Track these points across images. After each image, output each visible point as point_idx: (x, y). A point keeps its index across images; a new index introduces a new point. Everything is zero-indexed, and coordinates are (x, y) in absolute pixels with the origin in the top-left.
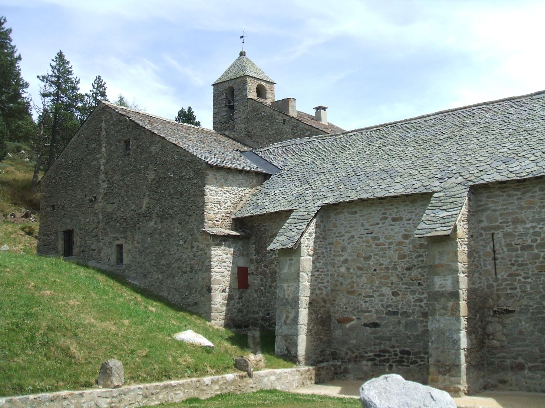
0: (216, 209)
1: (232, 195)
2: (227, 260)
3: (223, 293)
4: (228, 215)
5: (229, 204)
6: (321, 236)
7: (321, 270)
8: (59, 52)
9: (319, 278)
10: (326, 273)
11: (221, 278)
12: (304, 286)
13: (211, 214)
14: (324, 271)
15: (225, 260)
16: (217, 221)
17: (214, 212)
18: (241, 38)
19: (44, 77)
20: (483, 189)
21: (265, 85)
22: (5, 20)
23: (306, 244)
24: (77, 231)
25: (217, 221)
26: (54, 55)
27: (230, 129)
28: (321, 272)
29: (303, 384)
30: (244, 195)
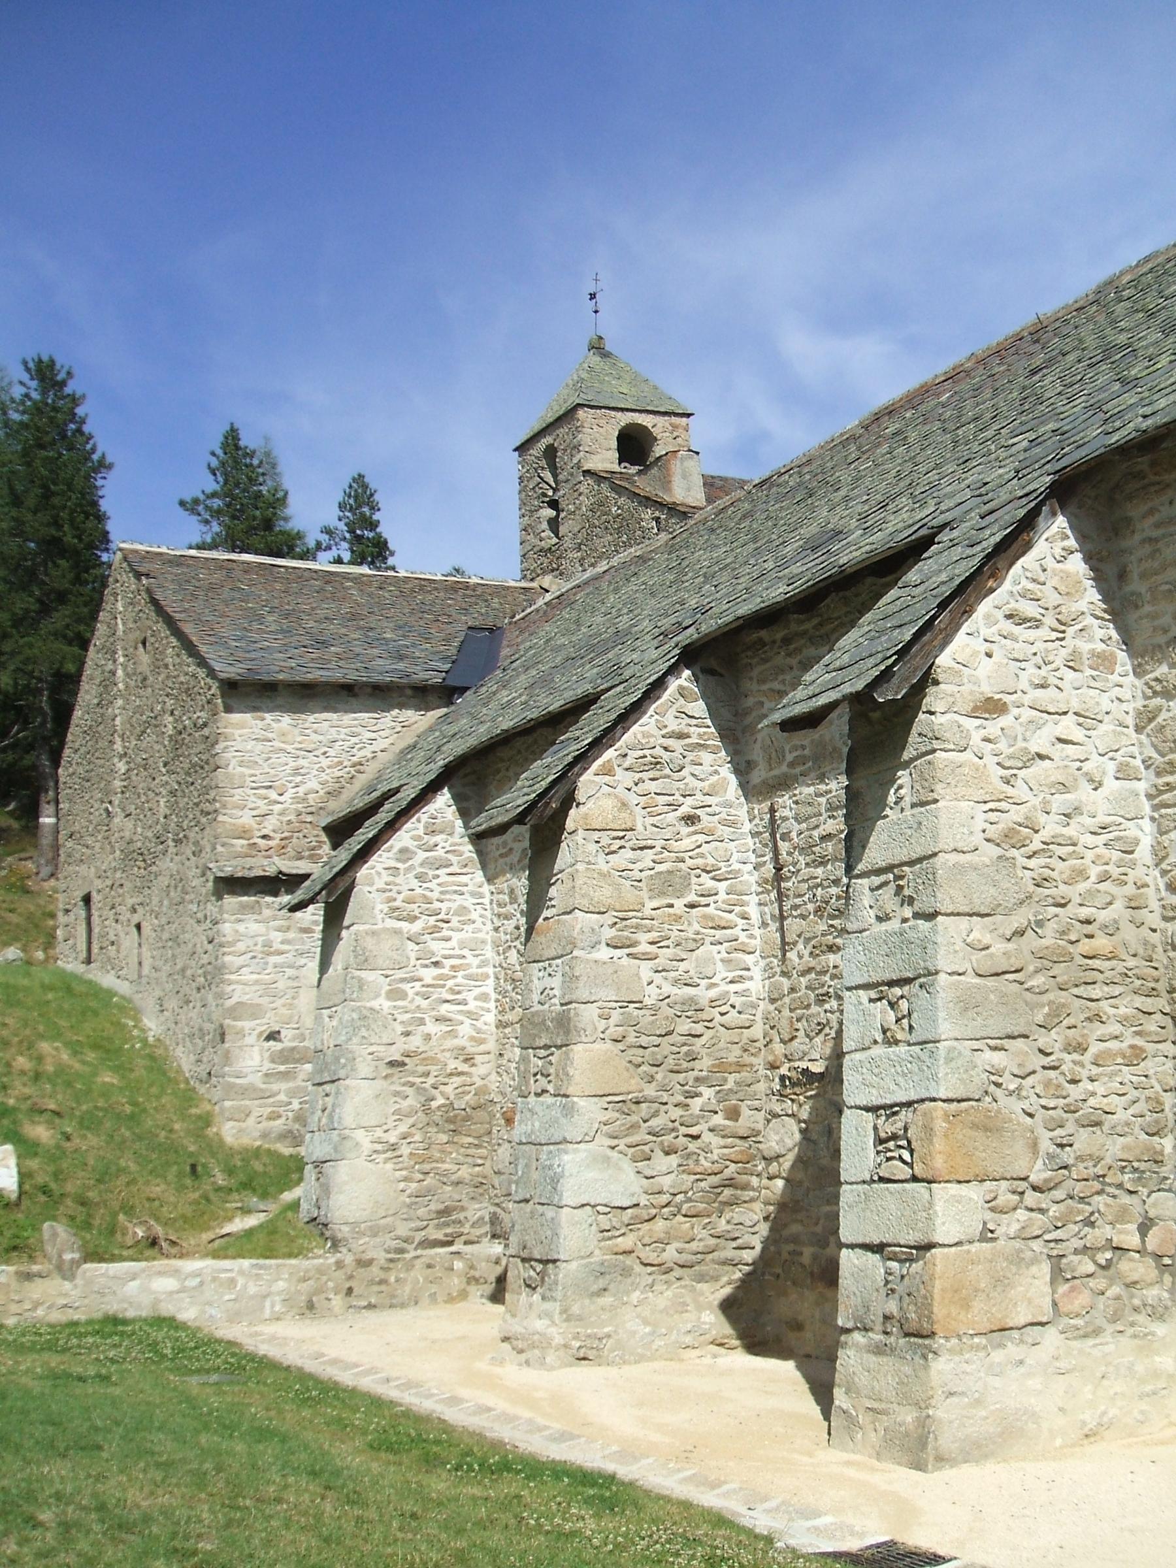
0: (261, 803)
1: (322, 758)
2: (285, 947)
3: (272, 1043)
4: (309, 818)
5: (313, 784)
6: (454, 859)
7: (448, 963)
8: (228, 428)
9: (443, 986)
10: (474, 970)
11: (264, 1001)
12: (365, 1012)
13: (246, 819)
14: (469, 965)
15: (277, 946)
16: (264, 837)
17: (255, 813)
18: (591, 299)
19: (196, 501)
20: (749, 653)
21: (649, 426)
22: (69, 373)
23: (382, 886)
24: (94, 894)
25: (264, 837)
26: (215, 442)
27: (553, 571)
28: (453, 967)
29: (311, 1306)
30: (370, 755)
